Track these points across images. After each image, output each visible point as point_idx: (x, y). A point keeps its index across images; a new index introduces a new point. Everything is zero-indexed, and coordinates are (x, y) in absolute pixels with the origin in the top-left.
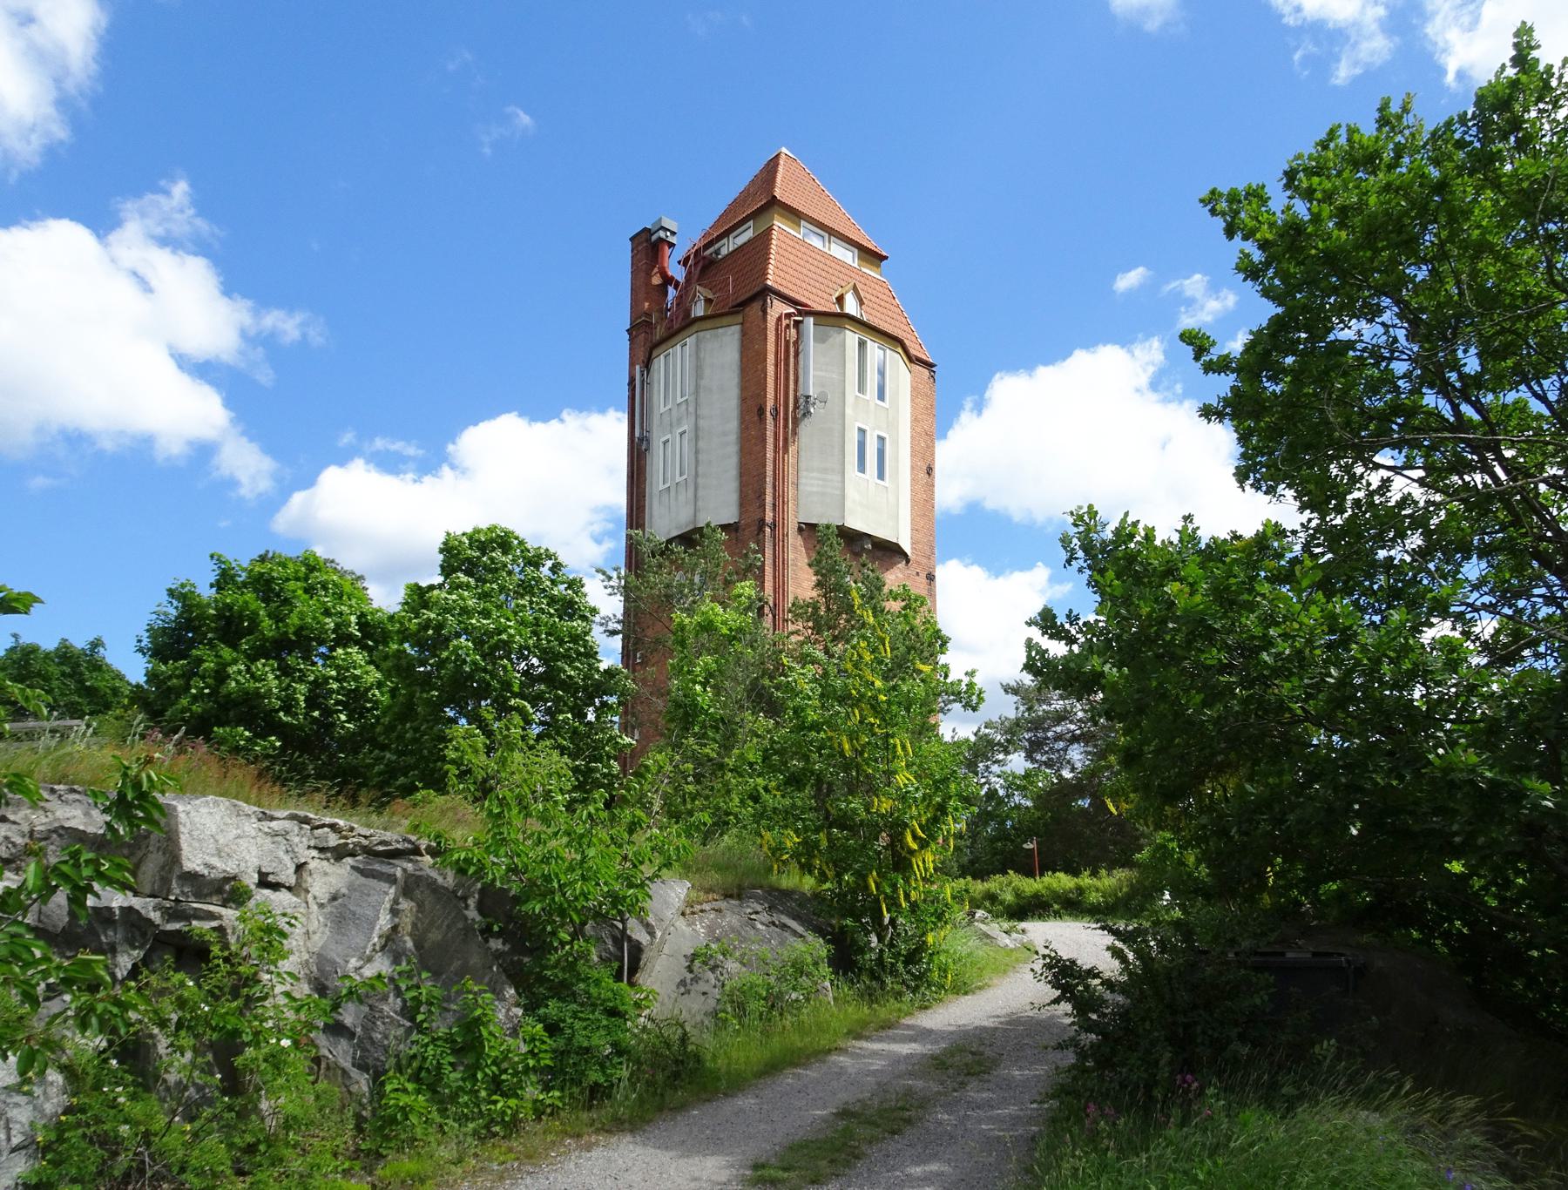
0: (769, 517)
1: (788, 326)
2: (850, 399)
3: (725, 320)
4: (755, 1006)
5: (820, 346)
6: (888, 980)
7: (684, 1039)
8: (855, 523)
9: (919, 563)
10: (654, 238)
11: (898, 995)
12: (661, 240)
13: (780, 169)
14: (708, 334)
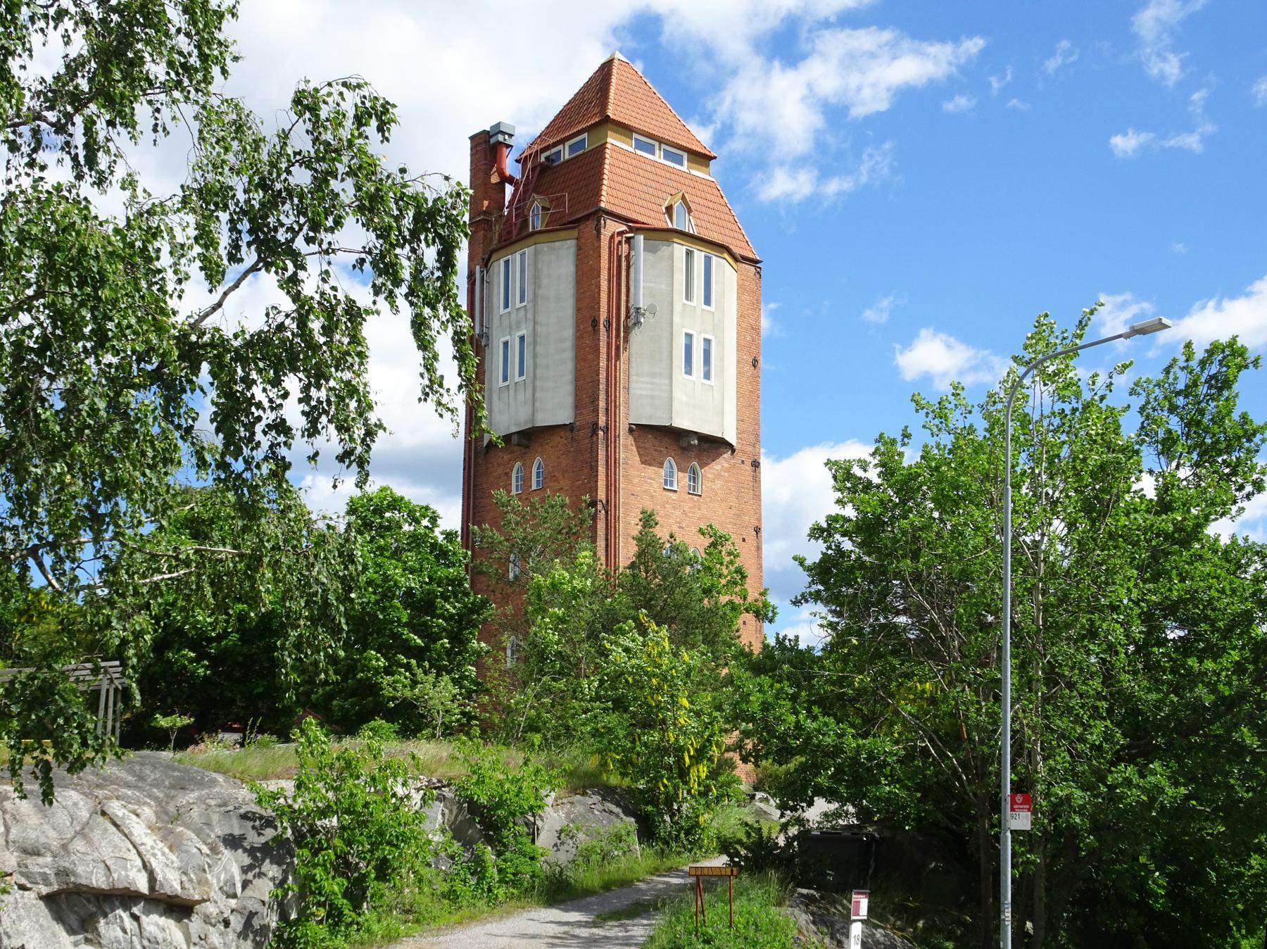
0: (602, 421)
1: (620, 243)
2: (677, 308)
3: (563, 234)
4: (595, 858)
5: (650, 257)
6: (674, 844)
7: (561, 873)
8: (681, 422)
9: (744, 452)
10: (493, 141)
11: (679, 853)
12: (500, 143)
13: (615, 71)
14: (545, 247)
